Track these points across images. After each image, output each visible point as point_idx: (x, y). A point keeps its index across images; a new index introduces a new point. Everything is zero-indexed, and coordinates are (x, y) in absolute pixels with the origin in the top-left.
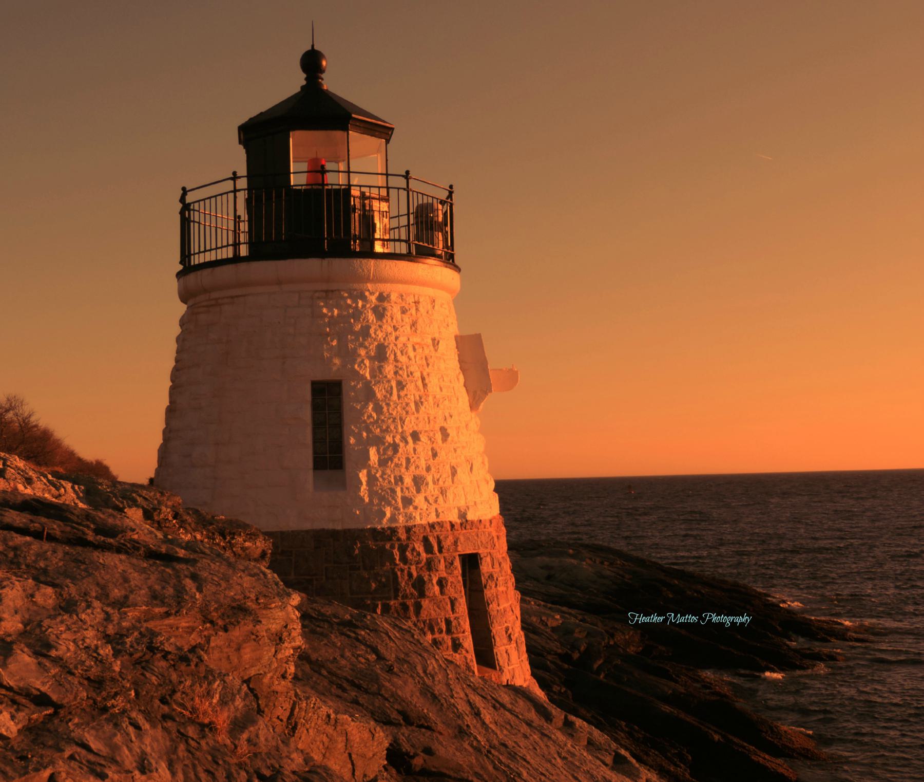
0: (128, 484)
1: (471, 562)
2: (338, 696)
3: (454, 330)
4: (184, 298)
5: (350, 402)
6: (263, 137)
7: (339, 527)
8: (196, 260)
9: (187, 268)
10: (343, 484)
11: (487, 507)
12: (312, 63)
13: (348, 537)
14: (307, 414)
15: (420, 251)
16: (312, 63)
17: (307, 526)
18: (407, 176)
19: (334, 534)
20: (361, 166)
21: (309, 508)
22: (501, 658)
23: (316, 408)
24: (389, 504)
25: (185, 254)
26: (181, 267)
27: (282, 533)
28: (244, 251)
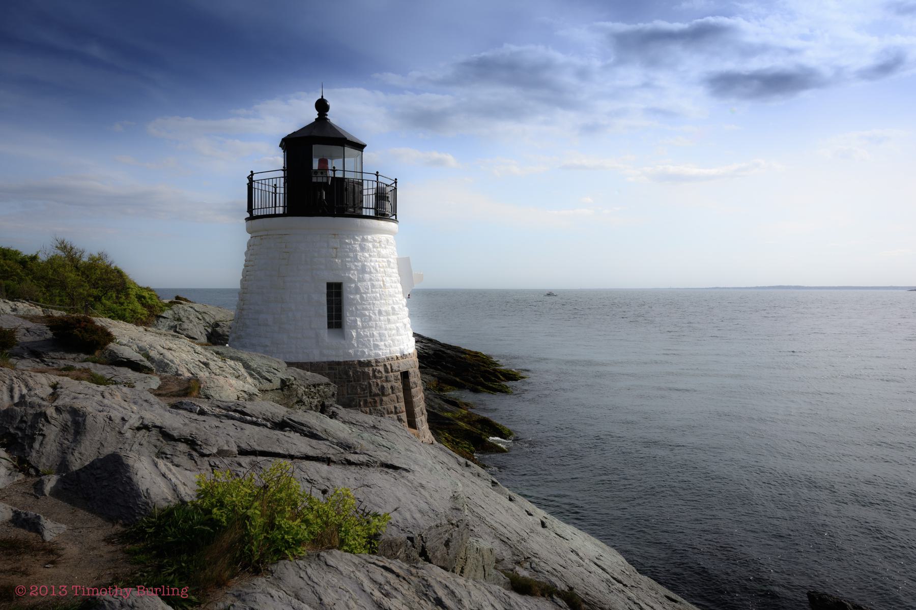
0: (440, 344)
1: (405, 375)
2: (761, 420)
3: (396, 255)
4: (249, 231)
5: (348, 296)
6: (297, 147)
7: (341, 360)
8: (255, 213)
9: (252, 218)
10: (343, 336)
11: (409, 346)
12: (322, 106)
13: (348, 364)
14: (324, 299)
15: (380, 215)
16: (322, 106)
17: (325, 359)
18: (377, 174)
19: (339, 363)
20: (344, 166)
21: (329, 348)
22: (419, 424)
23: (329, 295)
24: (367, 347)
25: (250, 208)
26: (248, 215)
27: (311, 363)
28: (280, 210)
